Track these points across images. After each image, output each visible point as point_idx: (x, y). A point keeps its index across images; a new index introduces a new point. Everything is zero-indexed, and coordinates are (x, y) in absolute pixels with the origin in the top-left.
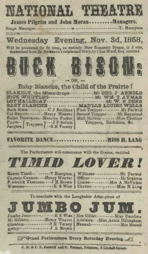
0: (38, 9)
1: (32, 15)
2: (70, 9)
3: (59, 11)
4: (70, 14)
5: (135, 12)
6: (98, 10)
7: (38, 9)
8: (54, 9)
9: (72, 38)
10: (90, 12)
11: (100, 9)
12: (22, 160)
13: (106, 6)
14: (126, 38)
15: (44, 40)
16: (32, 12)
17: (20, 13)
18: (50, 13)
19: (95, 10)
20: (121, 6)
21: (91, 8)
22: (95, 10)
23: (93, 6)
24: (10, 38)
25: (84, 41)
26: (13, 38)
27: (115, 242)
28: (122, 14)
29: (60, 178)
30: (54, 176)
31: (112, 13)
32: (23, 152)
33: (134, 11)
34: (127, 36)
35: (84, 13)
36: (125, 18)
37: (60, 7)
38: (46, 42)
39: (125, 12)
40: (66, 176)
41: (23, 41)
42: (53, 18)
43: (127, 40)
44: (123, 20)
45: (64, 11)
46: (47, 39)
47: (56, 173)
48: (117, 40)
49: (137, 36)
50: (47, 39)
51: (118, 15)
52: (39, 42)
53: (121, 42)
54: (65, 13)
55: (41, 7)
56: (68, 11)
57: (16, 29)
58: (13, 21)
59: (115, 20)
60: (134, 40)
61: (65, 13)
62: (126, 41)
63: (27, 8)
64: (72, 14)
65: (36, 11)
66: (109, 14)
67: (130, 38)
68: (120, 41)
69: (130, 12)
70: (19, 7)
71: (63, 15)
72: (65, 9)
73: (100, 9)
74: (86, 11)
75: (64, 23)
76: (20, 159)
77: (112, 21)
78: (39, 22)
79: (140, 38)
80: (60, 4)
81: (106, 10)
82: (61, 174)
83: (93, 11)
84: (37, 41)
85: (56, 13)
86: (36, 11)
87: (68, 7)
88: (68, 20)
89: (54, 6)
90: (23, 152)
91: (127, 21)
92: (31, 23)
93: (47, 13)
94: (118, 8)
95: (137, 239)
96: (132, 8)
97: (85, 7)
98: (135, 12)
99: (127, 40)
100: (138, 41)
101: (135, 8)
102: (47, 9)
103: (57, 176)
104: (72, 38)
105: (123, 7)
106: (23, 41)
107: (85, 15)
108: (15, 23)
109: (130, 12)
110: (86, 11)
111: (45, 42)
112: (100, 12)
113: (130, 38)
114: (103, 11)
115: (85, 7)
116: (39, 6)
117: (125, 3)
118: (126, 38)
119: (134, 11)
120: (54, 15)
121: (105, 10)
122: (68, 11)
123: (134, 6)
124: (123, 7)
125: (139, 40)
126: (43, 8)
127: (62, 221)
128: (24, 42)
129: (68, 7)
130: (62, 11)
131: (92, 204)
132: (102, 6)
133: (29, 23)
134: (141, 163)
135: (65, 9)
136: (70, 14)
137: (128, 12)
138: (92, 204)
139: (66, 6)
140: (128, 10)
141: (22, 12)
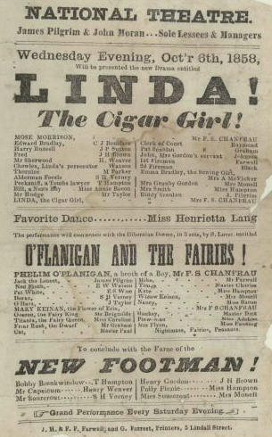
12: (61, 114)
15: (83, 56)
24: (24, 51)
25: (151, 59)
27: (212, 417)
29: (110, 389)
30: (99, 386)
34: (233, 52)
38: (88, 59)
40: (122, 386)
41: (135, 59)
44: (134, 37)
47: (104, 382)
48: (72, 56)
49: (249, 52)
52: (44, 58)
53: (222, 62)
60: (245, 60)
62: (230, 62)
76: (58, 113)
77: (158, 33)
80: (64, 100)
82: (115, 382)
84: (72, 56)
92: (52, 33)
95: (244, 408)
99: (233, 58)
100: (253, 60)
103: (105, 386)
106: (135, 59)
118: (230, 56)
125: (253, 59)
127: (113, 391)
128: (49, 58)
131: (85, 98)
138: (85, 98)
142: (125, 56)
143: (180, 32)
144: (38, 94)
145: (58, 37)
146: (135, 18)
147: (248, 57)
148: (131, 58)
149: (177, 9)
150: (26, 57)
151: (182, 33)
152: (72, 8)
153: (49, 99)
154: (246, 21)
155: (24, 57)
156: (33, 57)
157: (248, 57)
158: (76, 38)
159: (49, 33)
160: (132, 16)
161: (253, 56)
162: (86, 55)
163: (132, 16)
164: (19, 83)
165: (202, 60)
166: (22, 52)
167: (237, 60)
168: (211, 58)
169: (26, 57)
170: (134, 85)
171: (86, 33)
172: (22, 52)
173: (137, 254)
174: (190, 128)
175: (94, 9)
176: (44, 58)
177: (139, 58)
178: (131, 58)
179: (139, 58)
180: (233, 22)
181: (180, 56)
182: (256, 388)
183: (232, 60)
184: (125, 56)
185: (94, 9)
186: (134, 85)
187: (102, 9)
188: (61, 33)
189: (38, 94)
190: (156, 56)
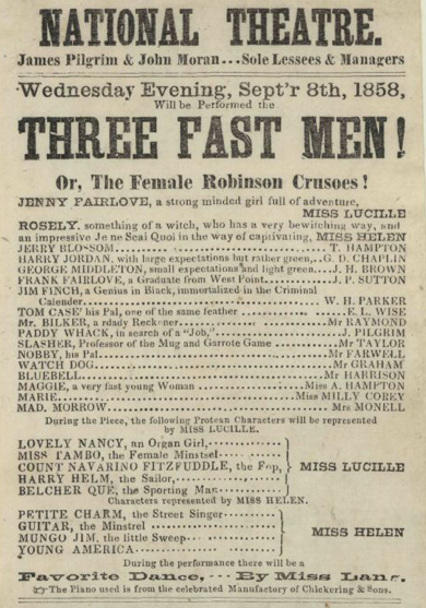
14: (268, 154)
15: (125, 90)
24: (30, 84)
25: (225, 92)
26: (38, 84)
32: (55, 590)
48: (106, 92)
52: (110, 95)
55: (130, 42)
58: (23, 56)
60: (381, 92)
62: (358, 94)
67: (369, 86)
68: (341, 94)
75: (151, 61)
77: (241, 59)
78: (96, 59)
79: (397, 86)
80: (73, 7)
84: (106, 92)
88: (161, 55)
90: (55, 590)
92: (74, 62)
99: (362, 89)
104: (192, 86)
106: (66, 93)
111: (127, 95)
113: (369, 86)
116: (134, 42)
118: (358, 85)
126: (126, 38)
134: (404, 145)
142: (184, 89)
145: (82, 68)
149: (336, 115)
150: (34, 94)
151: (279, 59)
153: (210, 120)
155: (30, 93)
156: (44, 94)
158: (111, 68)
159: (68, 63)
161: (393, 86)
164: (108, 123)
165: (313, 93)
166: (27, 87)
167: (369, 92)
168: (327, 90)
169: (34, 94)
170: (49, 152)
171: (128, 62)
172: (27, 87)
173: (303, 142)
174: (376, 27)
176: (266, 89)
178: (193, 92)
181: (279, 86)
183: (361, 93)
184: (184, 89)
186: (49, 152)
188: (87, 62)
190: (232, 87)
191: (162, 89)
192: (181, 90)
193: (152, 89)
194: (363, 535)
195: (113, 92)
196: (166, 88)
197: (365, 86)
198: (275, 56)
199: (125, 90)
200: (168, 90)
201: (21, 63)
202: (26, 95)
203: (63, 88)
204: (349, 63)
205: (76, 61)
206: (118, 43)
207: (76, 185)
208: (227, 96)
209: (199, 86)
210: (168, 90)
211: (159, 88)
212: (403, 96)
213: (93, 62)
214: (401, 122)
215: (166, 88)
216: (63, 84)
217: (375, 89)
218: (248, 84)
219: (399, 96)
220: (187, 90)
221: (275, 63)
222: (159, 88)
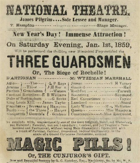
0: (35, 8)
1: (111, 14)
2: (65, 9)
3: (54, 10)
4: (64, 13)
5: (120, 12)
6: (86, 10)
7: (35, 8)
8: (50, 8)
9: (70, 43)
10: (79, 12)
11: (89, 8)
13: (94, 7)
15: (45, 45)
16: (30, 11)
17: (18, 12)
18: (46, 12)
19: (84, 10)
20: (76, 7)
21: (81, 8)
22: (84, 10)
23: (82, 6)
25: (81, 46)
28: (108, 14)
31: (56, 13)
33: (120, 11)
35: (75, 13)
36: (111, 17)
37: (56, 7)
38: (47, 46)
39: (111, 12)
41: (73, 46)
42: (93, 17)
43: (118, 45)
45: (58, 11)
46: (48, 44)
50: (48, 44)
51: (24, 14)
52: (40, 46)
54: (60, 12)
56: (62, 10)
57: (107, 26)
58: (22, 18)
59: (101, 18)
60: (124, 45)
61: (60, 12)
62: (116, 47)
63: (75, 7)
64: (66, 14)
65: (33, 10)
66: (96, 13)
69: (116, 12)
70: (18, 7)
71: (58, 14)
72: (60, 9)
73: (89, 8)
74: (76, 11)
77: (62, 20)
78: (45, 19)
81: (94, 10)
83: (82, 10)
84: (39, 45)
85: (52, 12)
86: (33, 10)
87: (63, 7)
89: (50, 6)
91: (111, 19)
92: (38, 20)
93: (43, 12)
94: (105, 8)
96: (118, 8)
97: (75, 7)
98: (120, 12)
99: (118, 45)
101: (120, 9)
102: (43, 8)
104: (70, 43)
105: (28, 7)
106: (73, 46)
107: (75, 15)
108: (24, 20)
109: (116, 12)
110: (76, 11)
111: (46, 46)
112: (89, 12)
114: (91, 11)
115: (75, 7)
117: (80, 4)
118: (116, 43)
119: (120, 11)
120: (49, 14)
121: (92, 10)
122: (62, 10)
123: (119, 7)
124: (28, 7)
129: (63, 7)
130: (57, 10)
132: (91, 7)
133: (36, 20)
135: (60, 9)
136: (64, 13)
137: (82, 12)
139: (61, 6)
140: (114, 10)
141: (102, 12)
142: (67, 44)
143: (74, 19)
144: (45, 60)
146: (131, 79)
147: (125, 44)
148: (71, 46)
151: (75, 19)
152: (32, 6)
154: (82, 71)
157: (125, 44)
160: (130, 79)
162: (46, 44)
163: (130, 79)
175: (44, 6)
176: (40, 46)
177: (75, 46)
178: (71, 46)
179: (75, 46)
180: (83, 77)
182: (101, 33)
184: (67, 44)
185: (44, 6)
187: (49, 6)
189: (45, 60)
191: (61, 45)
192: (66, 45)
193: (57, 44)
194: (45, 157)
195: (41, 45)
196: (62, 44)
197: (118, 44)
198: (74, 19)
199: (45, 45)
200: (62, 45)
201: (21, 20)
202: (15, 51)
203: (40, 44)
204: (101, 21)
205: (39, 20)
206: (42, 6)
207: (115, 95)
208: (81, 47)
209: (72, 44)
210: (62, 45)
211: (60, 44)
212: (112, 47)
213: (44, 20)
214: (11, 66)
215: (62, 44)
216: (40, 43)
217: (122, 45)
218: (22, 43)
219: (129, 47)
220: (68, 45)
221: (73, 21)
222: (60, 44)
